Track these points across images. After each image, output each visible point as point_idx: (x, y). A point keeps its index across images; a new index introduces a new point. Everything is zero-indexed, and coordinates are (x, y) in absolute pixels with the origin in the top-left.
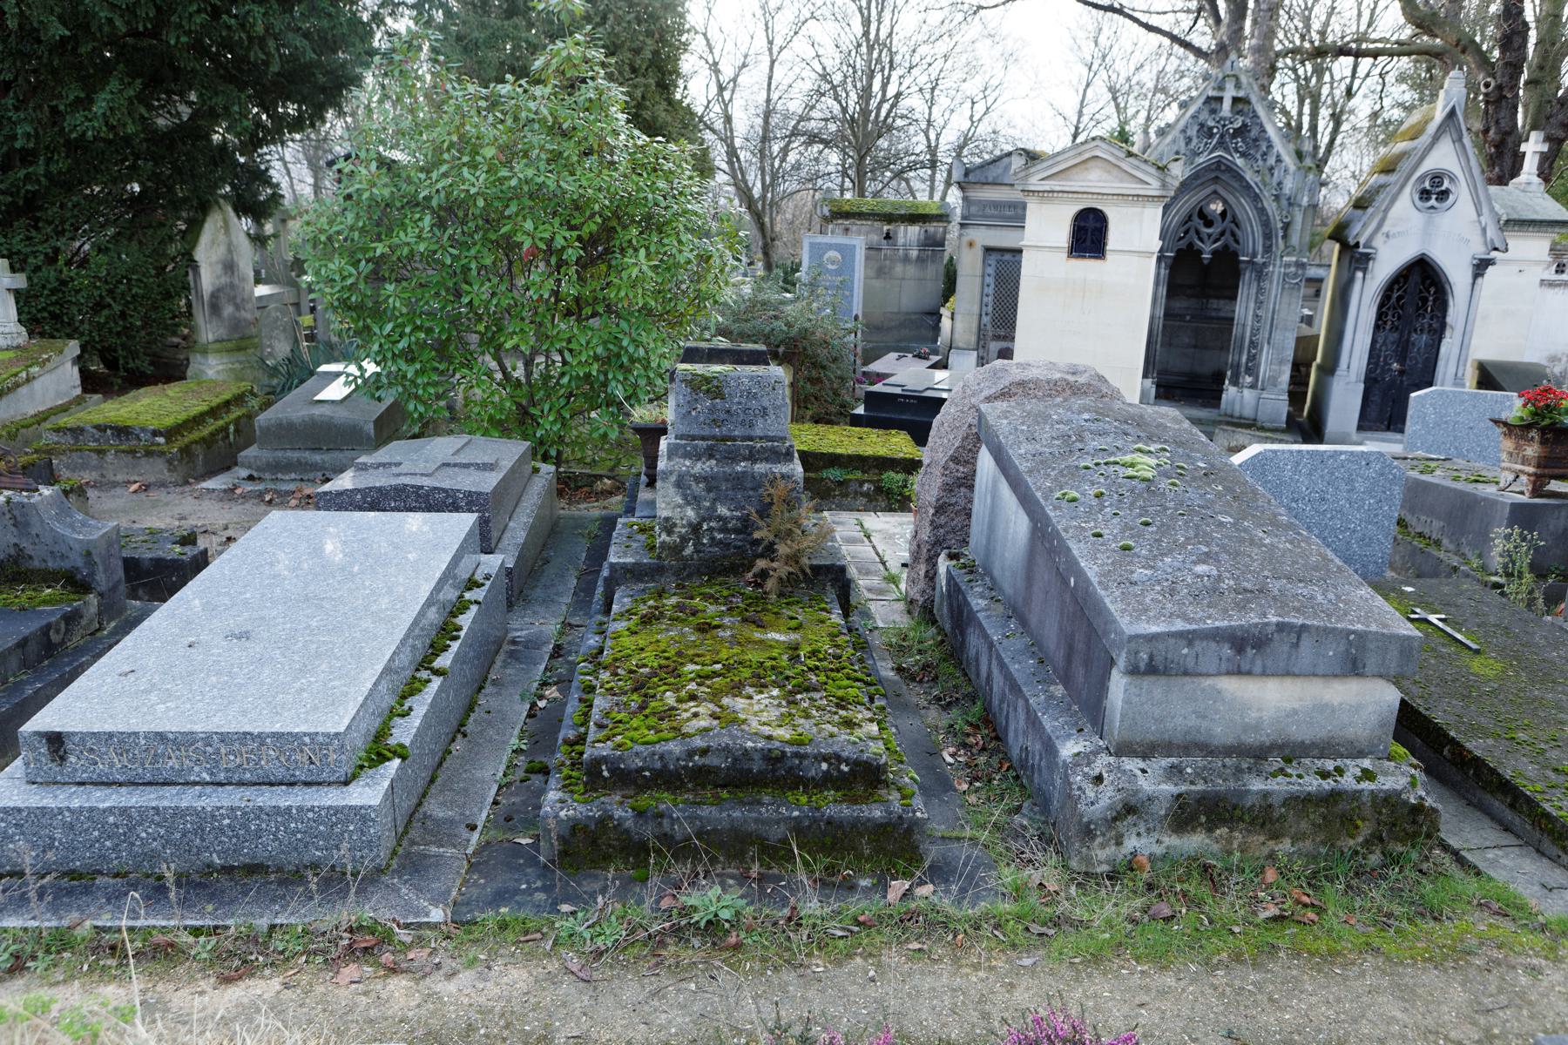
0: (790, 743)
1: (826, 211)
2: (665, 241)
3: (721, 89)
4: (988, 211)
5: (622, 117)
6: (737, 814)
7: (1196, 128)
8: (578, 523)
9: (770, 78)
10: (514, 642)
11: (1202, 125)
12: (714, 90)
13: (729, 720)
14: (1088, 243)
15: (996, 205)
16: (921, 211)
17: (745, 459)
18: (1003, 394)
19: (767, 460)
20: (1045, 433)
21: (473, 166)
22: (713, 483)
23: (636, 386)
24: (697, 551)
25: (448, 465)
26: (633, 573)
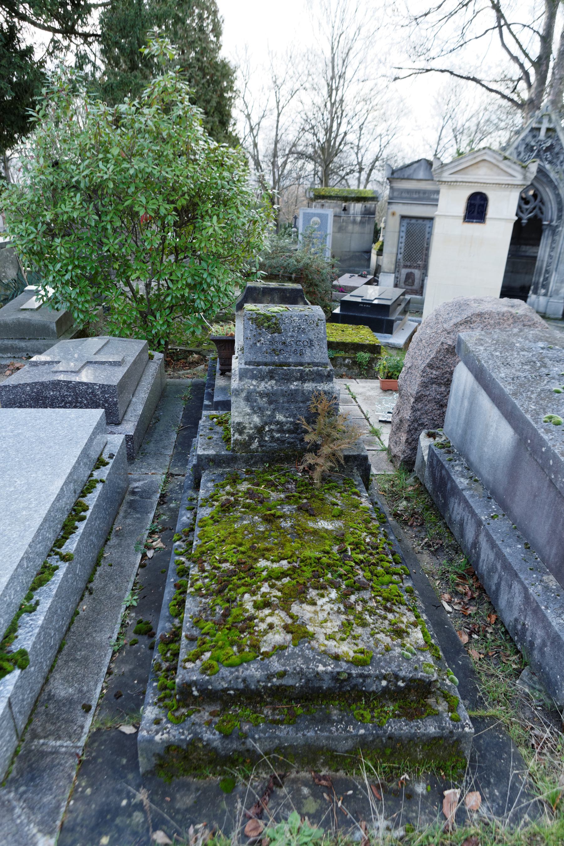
0: (355, 663)
1: (312, 195)
2: (229, 211)
3: (252, 129)
4: (404, 195)
5: (201, 129)
6: (311, 734)
7: (524, 146)
8: (178, 389)
9: (278, 121)
10: (133, 493)
11: (527, 145)
12: (248, 129)
13: (298, 632)
14: (476, 213)
15: (409, 191)
16: (363, 195)
17: (297, 380)
18: (466, 322)
19: (313, 380)
20: (516, 359)
21: (106, 161)
22: (274, 398)
23: (212, 303)
24: (261, 446)
25: (91, 362)
26: (215, 461)
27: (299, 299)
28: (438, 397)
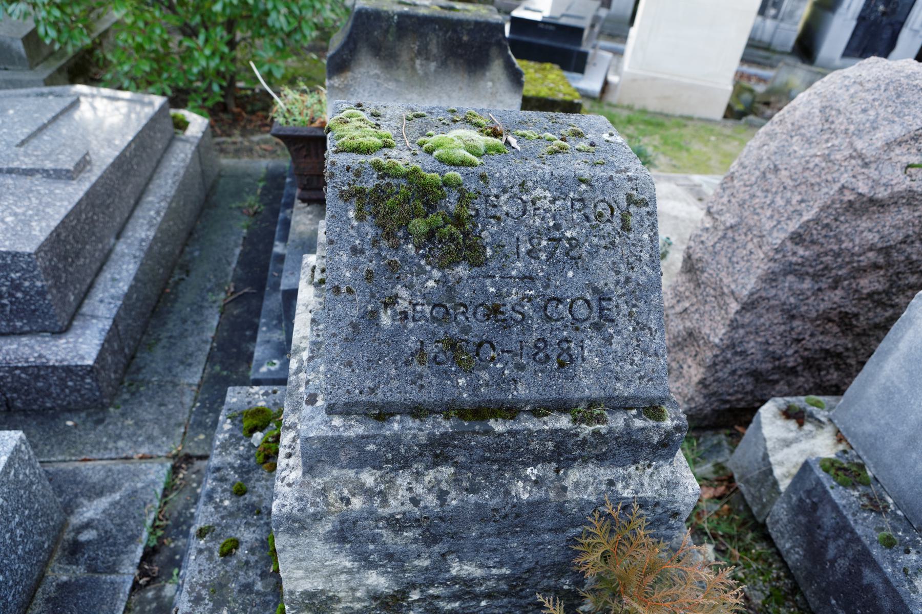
8: (240, 183)
17: (538, 459)
23: (300, 19)
27: (494, 51)
28: (792, 300)
